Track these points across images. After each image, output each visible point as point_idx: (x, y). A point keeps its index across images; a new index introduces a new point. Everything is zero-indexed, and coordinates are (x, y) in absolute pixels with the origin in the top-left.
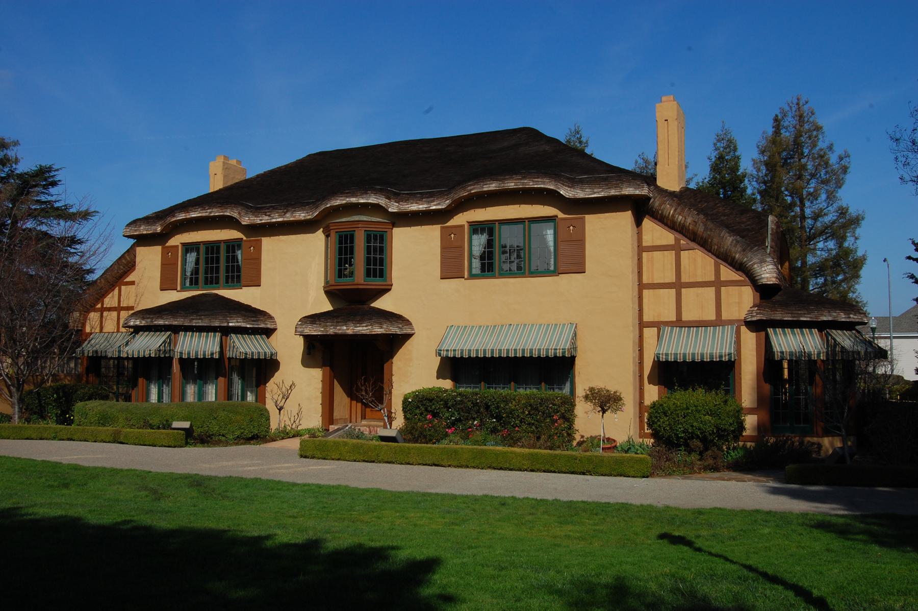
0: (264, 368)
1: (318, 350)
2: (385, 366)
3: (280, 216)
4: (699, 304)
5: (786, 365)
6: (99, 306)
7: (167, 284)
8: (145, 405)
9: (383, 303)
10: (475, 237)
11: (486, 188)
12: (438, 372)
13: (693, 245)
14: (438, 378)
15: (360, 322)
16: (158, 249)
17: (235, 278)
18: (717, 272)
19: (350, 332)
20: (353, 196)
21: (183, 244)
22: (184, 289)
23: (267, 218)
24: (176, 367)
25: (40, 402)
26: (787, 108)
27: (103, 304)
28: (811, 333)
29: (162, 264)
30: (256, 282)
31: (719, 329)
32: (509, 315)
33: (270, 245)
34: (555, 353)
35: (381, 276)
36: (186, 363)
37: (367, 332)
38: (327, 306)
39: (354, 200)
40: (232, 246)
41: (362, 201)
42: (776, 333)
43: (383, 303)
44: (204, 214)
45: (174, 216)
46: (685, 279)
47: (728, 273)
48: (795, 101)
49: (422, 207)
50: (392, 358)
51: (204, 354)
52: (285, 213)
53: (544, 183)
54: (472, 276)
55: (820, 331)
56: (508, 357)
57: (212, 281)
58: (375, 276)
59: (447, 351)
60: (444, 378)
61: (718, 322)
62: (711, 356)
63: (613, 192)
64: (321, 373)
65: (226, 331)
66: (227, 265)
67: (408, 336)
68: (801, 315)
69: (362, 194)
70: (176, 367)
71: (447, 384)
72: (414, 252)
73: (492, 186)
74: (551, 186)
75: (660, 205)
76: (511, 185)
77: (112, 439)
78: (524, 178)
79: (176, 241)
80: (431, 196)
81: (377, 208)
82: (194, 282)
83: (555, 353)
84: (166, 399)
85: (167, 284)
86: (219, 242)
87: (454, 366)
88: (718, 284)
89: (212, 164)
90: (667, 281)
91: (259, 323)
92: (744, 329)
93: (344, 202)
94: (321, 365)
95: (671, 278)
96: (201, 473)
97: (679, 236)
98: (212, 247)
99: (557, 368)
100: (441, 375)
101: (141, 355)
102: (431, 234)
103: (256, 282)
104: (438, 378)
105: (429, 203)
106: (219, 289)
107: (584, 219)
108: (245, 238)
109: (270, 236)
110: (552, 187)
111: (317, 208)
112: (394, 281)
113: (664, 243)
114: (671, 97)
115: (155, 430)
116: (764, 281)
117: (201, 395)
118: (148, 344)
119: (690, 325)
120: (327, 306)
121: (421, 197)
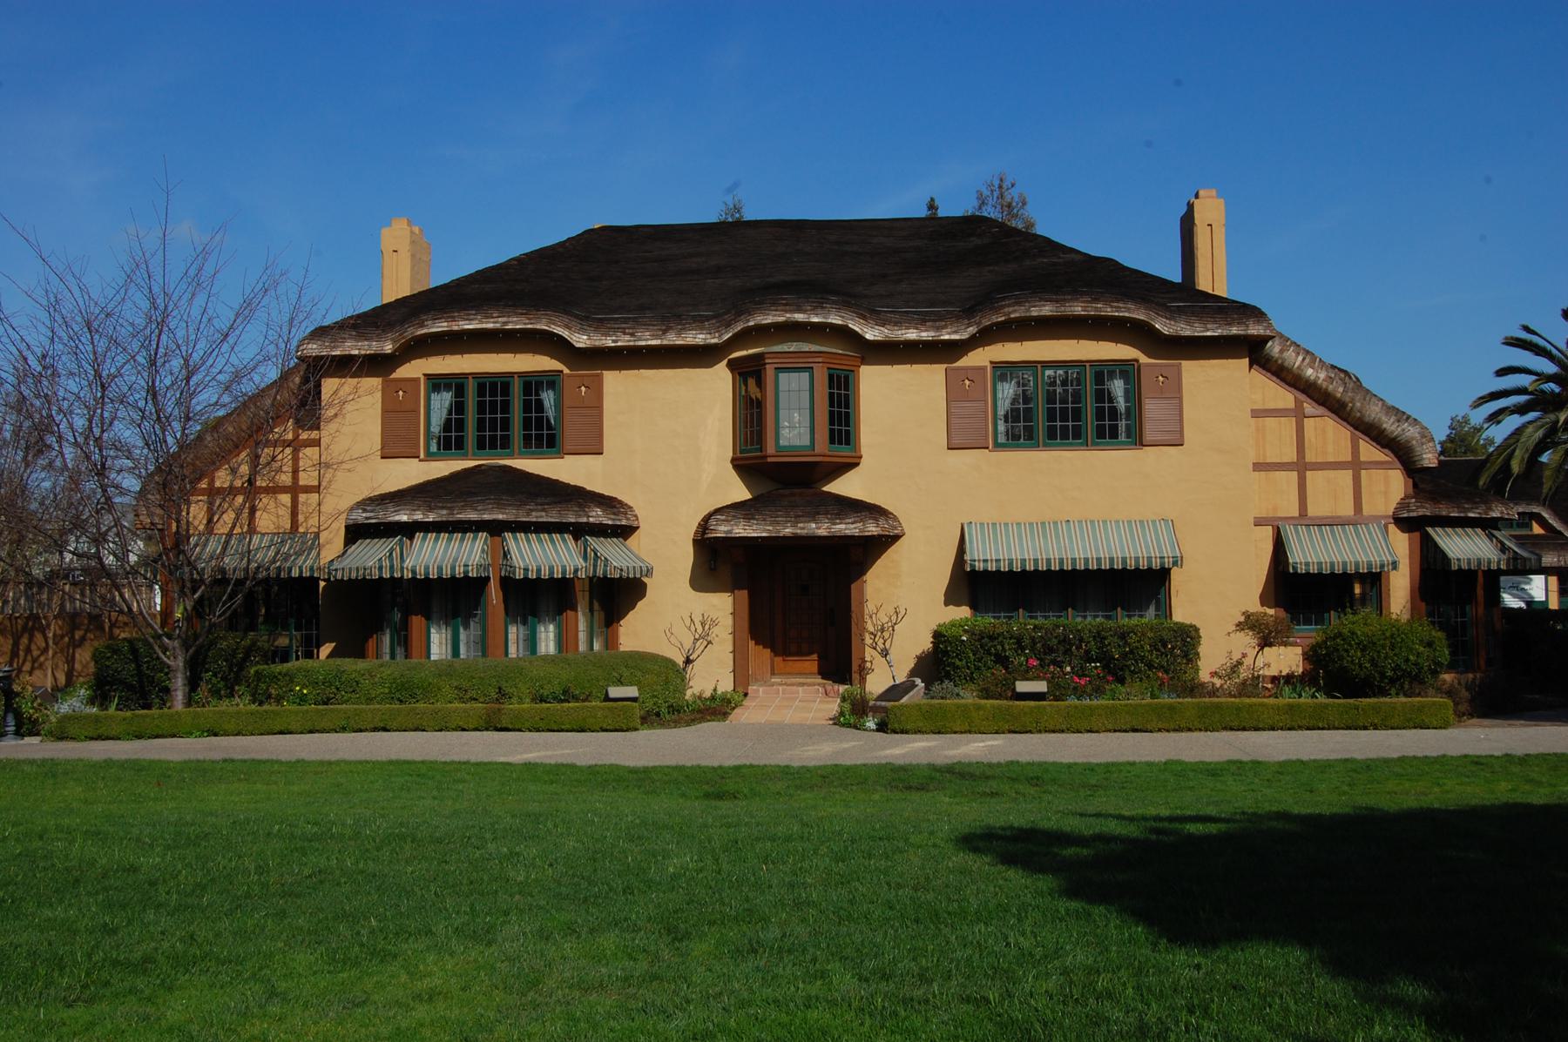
0: (616, 596)
1: (717, 559)
2: (853, 586)
3: (655, 337)
4: (1330, 494)
5: (1480, 579)
6: (204, 485)
7: (393, 448)
8: (309, 663)
9: (845, 486)
10: (999, 386)
11: (1035, 312)
12: (946, 594)
13: (1321, 410)
14: (947, 604)
15: (813, 517)
16: (375, 382)
17: (546, 439)
18: (1355, 451)
19: (822, 532)
20: (799, 310)
21: (428, 377)
22: (430, 456)
23: (627, 338)
24: (494, 593)
25: (138, 667)
26: (986, 193)
27: (212, 481)
28: (564, 540)
29: (385, 411)
30: (593, 446)
31: (1362, 529)
32: (1063, 508)
33: (617, 384)
34: (466, 572)
35: (848, 443)
36: (510, 585)
37: (856, 532)
38: (741, 493)
39: (800, 317)
40: (534, 383)
41: (816, 320)
42: (516, 539)
43: (845, 486)
44: (490, 326)
45: (422, 326)
46: (1310, 457)
47: (1370, 451)
48: (996, 183)
49: (926, 335)
50: (863, 572)
51: (564, 572)
52: (665, 332)
53: (1128, 310)
54: (998, 446)
55: (576, 539)
56: (1049, 571)
57: (503, 444)
58: (840, 443)
59: (985, 561)
60: (958, 605)
61: (1358, 519)
62: (1370, 565)
63: (1235, 331)
64: (730, 600)
65: (495, 529)
66: (499, 416)
67: (897, 538)
68: (1470, 510)
69: (815, 308)
70: (494, 593)
71: (963, 612)
72: (900, 408)
73: (1046, 310)
74: (1140, 315)
75: (1281, 351)
76: (1078, 309)
77: (482, 723)
78: (1096, 300)
79: (415, 369)
80: (937, 320)
81: (844, 334)
82: (450, 442)
83: (466, 572)
84: (596, 646)
85: (393, 448)
86: (511, 375)
87: (971, 584)
88: (1356, 465)
89: (385, 232)
90: (1285, 460)
91: (599, 518)
92: (1392, 527)
93: (781, 319)
94: (732, 587)
95: (1290, 455)
96: (704, 763)
97: (1302, 397)
98: (493, 386)
99: (1144, 585)
100: (951, 598)
101: (447, 574)
102: (929, 379)
103: (593, 446)
104: (947, 604)
105: (938, 329)
106: (511, 456)
107: (600, 378)
108: (566, 371)
109: (620, 369)
110: (1142, 317)
111: (728, 325)
112: (864, 451)
113: (1280, 405)
114: (1214, 193)
115: (409, 703)
116: (1426, 464)
117: (532, 643)
118: (371, 558)
119: (1321, 523)
120: (741, 493)
121: (922, 321)
